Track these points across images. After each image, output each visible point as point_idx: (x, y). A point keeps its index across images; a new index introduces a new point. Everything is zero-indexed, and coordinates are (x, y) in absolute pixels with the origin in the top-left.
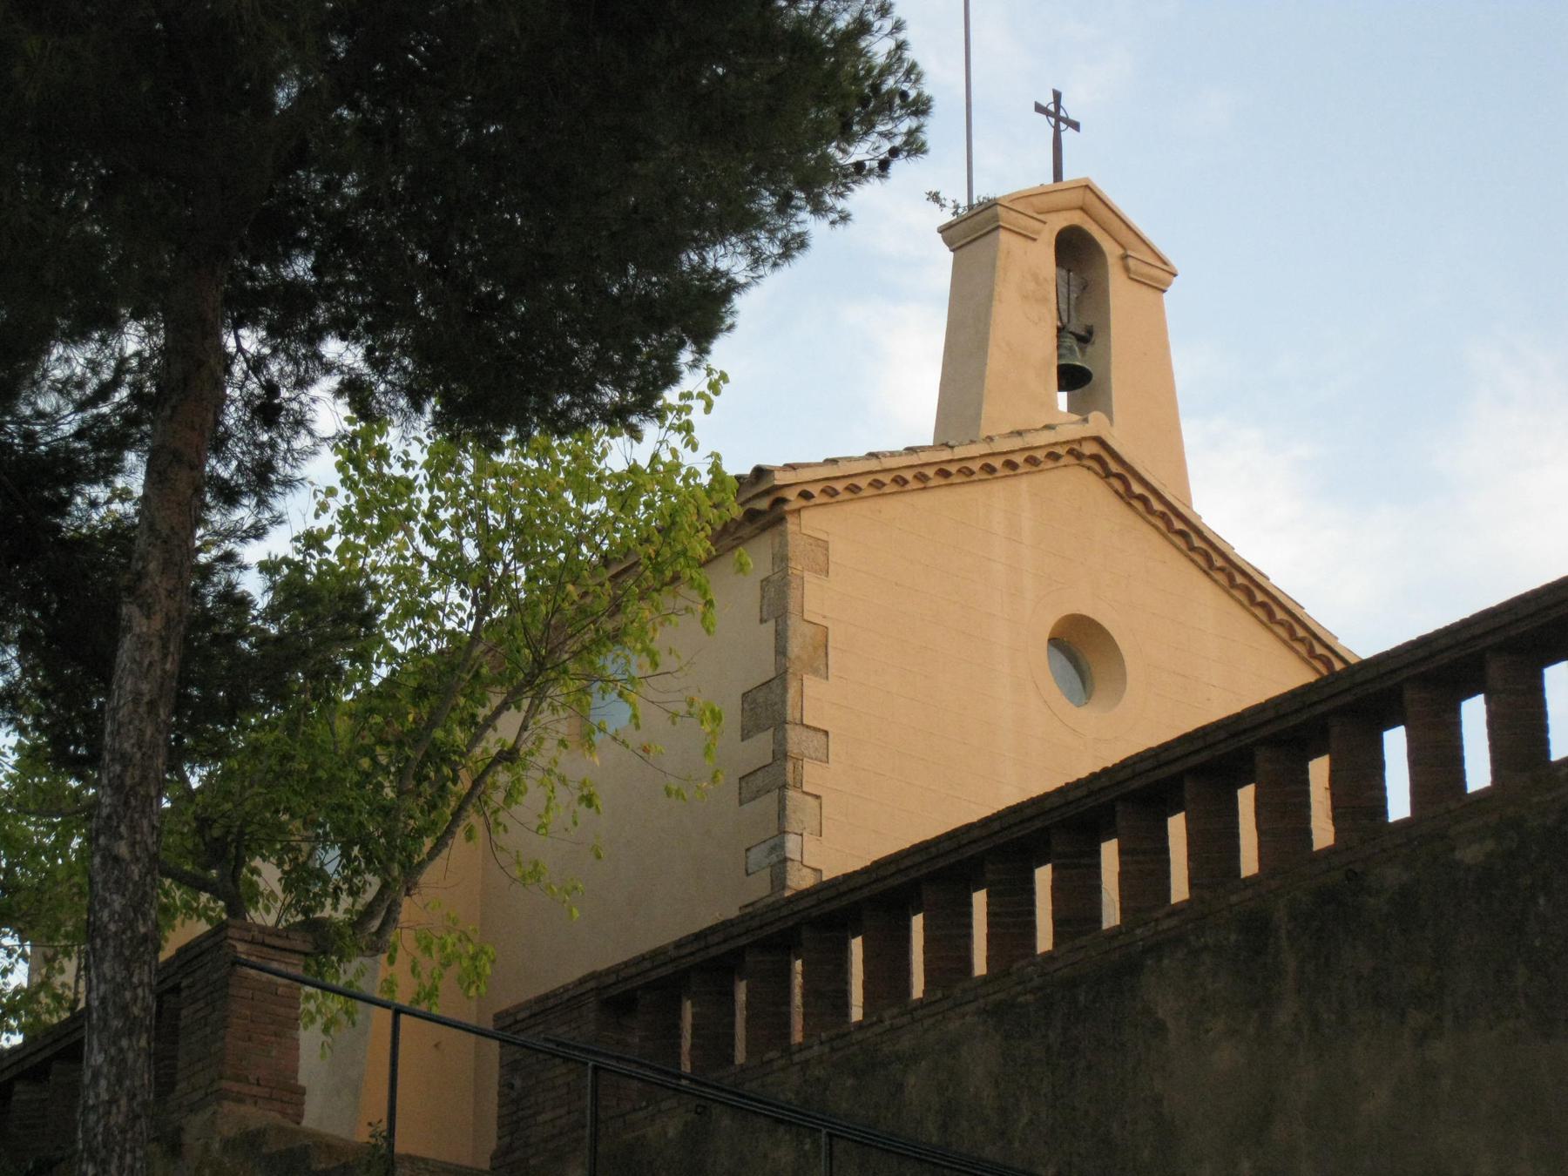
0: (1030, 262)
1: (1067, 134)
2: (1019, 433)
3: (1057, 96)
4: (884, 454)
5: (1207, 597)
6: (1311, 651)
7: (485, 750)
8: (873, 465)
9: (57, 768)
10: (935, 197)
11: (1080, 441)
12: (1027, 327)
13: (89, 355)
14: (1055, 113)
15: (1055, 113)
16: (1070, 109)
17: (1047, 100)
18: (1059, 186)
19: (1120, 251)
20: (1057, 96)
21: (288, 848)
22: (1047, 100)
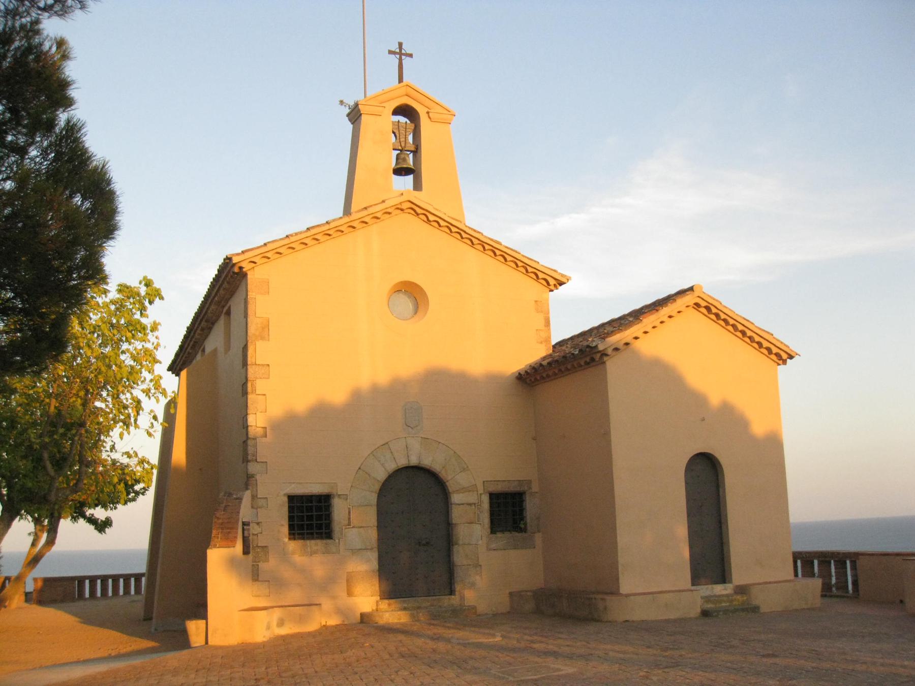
0: (381, 126)
1: (406, 61)
2: (366, 208)
3: (400, 45)
4: (292, 235)
5: (473, 256)
6: (527, 271)
7: (281, 623)
8: (287, 241)
9: (59, 361)
10: (342, 102)
11: (401, 203)
12: (380, 153)
13: (126, 362)
14: (400, 53)
15: (400, 53)
16: (407, 49)
17: (395, 48)
18: (401, 84)
19: (427, 110)
20: (400, 45)
21: (25, 476)
22: (395, 48)
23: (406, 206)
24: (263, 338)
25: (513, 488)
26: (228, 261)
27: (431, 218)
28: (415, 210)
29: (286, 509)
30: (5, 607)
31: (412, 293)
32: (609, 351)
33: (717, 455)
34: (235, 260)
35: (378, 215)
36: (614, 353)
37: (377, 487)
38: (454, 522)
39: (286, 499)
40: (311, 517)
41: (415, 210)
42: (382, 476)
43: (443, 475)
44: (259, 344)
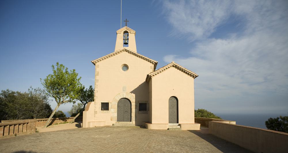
20: (126, 19)
23: (124, 50)
24: (97, 75)
25: (144, 102)
26: (148, 75)
27: (151, 62)
28: (126, 51)
29: (101, 105)
30: (199, 109)
31: (126, 67)
32: (152, 76)
33: (176, 96)
34: (149, 75)
35: (119, 52)
36: (153, 76)
37: (117, 102)
38: (52, 109)
39: (101, 104)
40: (105, 106)
41: (126, 51)
42: (118, 100)
43: (130, 99)
44: (97, 76)
